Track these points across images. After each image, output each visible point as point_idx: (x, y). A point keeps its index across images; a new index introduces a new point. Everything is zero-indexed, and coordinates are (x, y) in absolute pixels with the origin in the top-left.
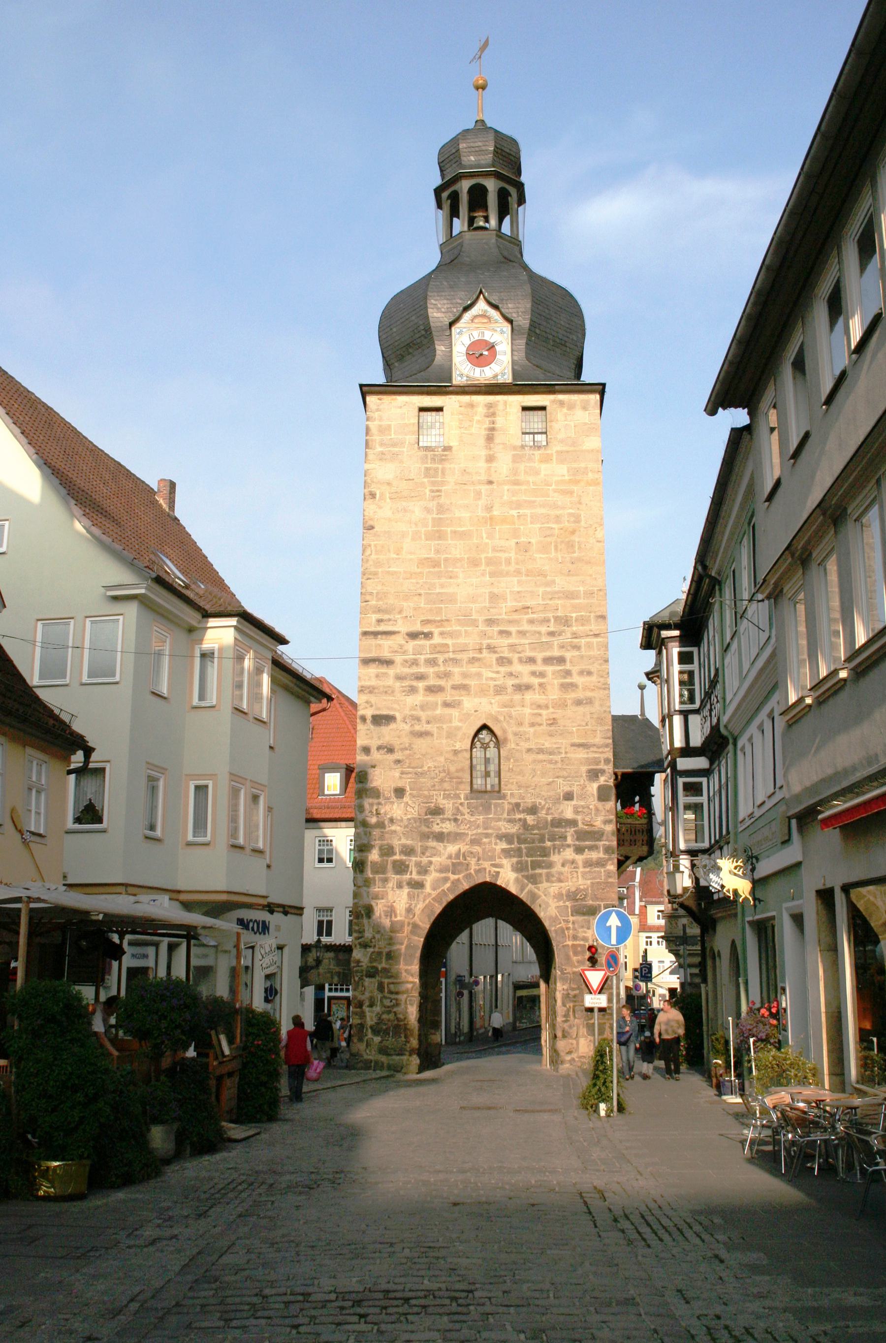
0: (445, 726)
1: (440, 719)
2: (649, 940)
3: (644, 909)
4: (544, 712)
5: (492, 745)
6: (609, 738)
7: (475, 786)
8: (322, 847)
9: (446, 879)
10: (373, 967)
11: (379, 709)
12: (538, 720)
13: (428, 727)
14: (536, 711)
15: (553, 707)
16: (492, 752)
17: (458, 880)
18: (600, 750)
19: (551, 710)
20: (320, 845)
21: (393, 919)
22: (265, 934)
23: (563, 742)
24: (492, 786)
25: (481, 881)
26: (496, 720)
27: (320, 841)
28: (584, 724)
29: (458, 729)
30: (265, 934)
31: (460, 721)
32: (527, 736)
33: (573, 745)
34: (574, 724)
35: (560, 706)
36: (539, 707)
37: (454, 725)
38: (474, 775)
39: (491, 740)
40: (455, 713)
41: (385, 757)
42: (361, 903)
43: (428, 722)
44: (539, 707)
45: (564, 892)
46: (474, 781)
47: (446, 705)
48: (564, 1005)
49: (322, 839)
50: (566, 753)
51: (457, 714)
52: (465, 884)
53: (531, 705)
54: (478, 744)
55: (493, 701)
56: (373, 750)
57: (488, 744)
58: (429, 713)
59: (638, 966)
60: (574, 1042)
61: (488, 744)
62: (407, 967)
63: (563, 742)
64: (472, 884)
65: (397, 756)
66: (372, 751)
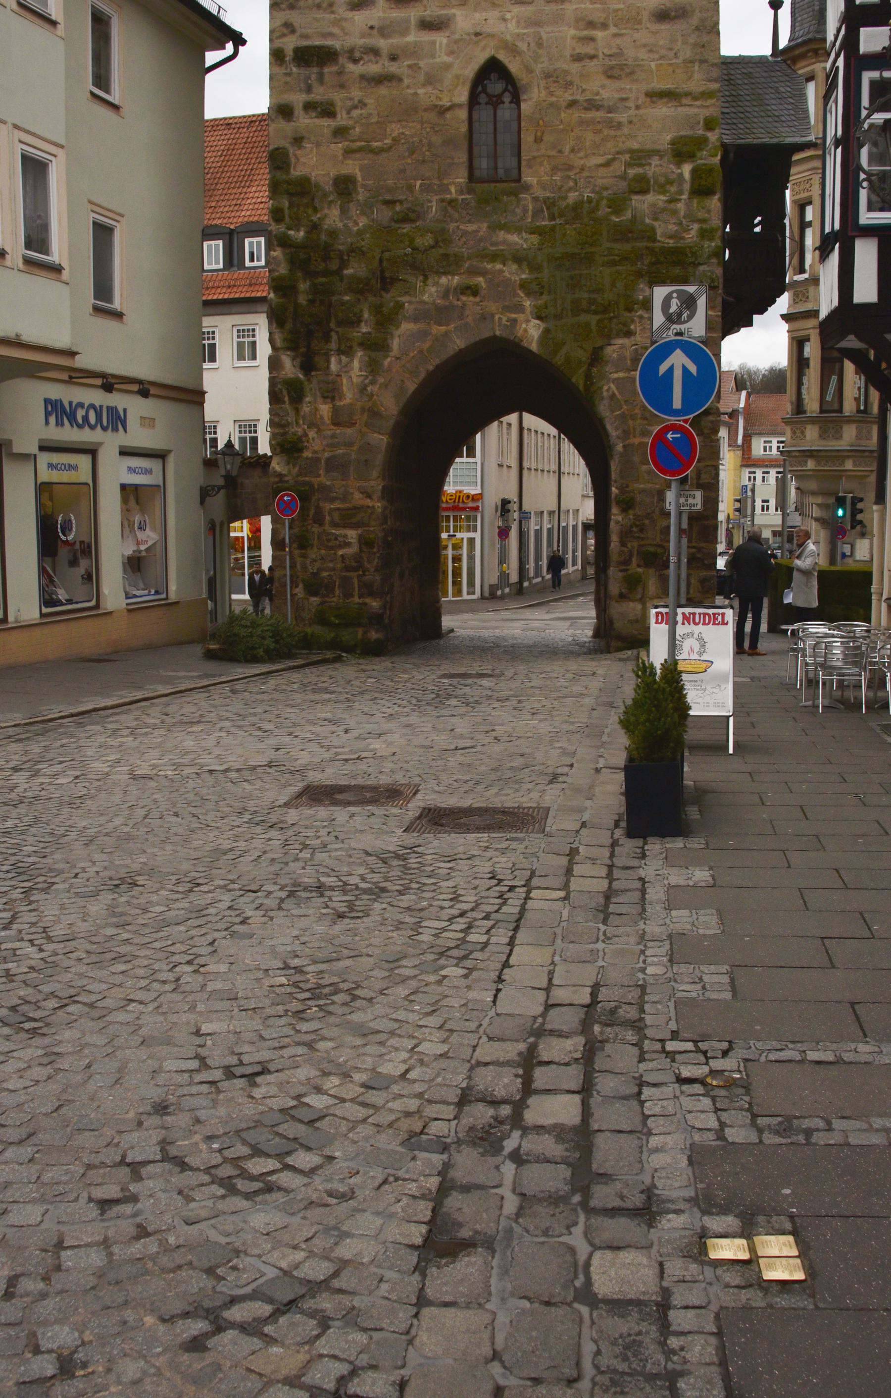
0: (422, 64)
1: (413, 51)
2: (768, 445)
3: (747, 438)
4: (599, 34)
5: (507, 98)
6: (715, 80)
7: (477, 173)
8: (241, 340)
9: (423, 334)
10: (305, 483)
11: (305, 37)
12: (589, 49)
13: (394, 68)
14: (585, 33)
15: (615, 25)
16: (505, 112)
17: (446, 334)
18: (698, 103)
19: (613, 30)
20: (239, 337)
21: (338, 403)
22: (116, 430)
23: (634, 89)
24: (507, 171)
25: (487, 334)
26: (513, 50)
27: (238, 331)
28: (672, 54)
29: (447, 67)
30: (116, 430)
31: (451, 53)
32: (569, 78)
33: (648, 94)
34: (652, 56)
35: (628, 21)
36: (591, 25)
37: (438, 60)
38: (476, 150)
39: (506, 90)
40: (440, 39)
41: (318, 121)
42: (281, 376)
43: (393, 58)
44: (591, 25)
45: (628, 354)
46: (476, 162)
47: (427, 25)
48: (623, 543)
49: (241, 328)
50: (638, 107)
51: (445, 41)
52: (458, 341)
53: (577, 21)
54: (483, 99)
55: (508, 16)
56: (299, 111)
57: (500, 96)
58: (395, 41)
59: (818, 244)
60: (639, 607)
61: (500, 96)
62: (368, 502)
63: (634, 89)
64: (474, 339)
65: (342, 119)
66: (296, 113)
